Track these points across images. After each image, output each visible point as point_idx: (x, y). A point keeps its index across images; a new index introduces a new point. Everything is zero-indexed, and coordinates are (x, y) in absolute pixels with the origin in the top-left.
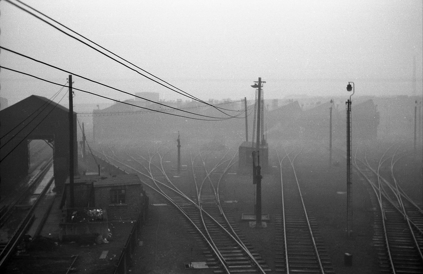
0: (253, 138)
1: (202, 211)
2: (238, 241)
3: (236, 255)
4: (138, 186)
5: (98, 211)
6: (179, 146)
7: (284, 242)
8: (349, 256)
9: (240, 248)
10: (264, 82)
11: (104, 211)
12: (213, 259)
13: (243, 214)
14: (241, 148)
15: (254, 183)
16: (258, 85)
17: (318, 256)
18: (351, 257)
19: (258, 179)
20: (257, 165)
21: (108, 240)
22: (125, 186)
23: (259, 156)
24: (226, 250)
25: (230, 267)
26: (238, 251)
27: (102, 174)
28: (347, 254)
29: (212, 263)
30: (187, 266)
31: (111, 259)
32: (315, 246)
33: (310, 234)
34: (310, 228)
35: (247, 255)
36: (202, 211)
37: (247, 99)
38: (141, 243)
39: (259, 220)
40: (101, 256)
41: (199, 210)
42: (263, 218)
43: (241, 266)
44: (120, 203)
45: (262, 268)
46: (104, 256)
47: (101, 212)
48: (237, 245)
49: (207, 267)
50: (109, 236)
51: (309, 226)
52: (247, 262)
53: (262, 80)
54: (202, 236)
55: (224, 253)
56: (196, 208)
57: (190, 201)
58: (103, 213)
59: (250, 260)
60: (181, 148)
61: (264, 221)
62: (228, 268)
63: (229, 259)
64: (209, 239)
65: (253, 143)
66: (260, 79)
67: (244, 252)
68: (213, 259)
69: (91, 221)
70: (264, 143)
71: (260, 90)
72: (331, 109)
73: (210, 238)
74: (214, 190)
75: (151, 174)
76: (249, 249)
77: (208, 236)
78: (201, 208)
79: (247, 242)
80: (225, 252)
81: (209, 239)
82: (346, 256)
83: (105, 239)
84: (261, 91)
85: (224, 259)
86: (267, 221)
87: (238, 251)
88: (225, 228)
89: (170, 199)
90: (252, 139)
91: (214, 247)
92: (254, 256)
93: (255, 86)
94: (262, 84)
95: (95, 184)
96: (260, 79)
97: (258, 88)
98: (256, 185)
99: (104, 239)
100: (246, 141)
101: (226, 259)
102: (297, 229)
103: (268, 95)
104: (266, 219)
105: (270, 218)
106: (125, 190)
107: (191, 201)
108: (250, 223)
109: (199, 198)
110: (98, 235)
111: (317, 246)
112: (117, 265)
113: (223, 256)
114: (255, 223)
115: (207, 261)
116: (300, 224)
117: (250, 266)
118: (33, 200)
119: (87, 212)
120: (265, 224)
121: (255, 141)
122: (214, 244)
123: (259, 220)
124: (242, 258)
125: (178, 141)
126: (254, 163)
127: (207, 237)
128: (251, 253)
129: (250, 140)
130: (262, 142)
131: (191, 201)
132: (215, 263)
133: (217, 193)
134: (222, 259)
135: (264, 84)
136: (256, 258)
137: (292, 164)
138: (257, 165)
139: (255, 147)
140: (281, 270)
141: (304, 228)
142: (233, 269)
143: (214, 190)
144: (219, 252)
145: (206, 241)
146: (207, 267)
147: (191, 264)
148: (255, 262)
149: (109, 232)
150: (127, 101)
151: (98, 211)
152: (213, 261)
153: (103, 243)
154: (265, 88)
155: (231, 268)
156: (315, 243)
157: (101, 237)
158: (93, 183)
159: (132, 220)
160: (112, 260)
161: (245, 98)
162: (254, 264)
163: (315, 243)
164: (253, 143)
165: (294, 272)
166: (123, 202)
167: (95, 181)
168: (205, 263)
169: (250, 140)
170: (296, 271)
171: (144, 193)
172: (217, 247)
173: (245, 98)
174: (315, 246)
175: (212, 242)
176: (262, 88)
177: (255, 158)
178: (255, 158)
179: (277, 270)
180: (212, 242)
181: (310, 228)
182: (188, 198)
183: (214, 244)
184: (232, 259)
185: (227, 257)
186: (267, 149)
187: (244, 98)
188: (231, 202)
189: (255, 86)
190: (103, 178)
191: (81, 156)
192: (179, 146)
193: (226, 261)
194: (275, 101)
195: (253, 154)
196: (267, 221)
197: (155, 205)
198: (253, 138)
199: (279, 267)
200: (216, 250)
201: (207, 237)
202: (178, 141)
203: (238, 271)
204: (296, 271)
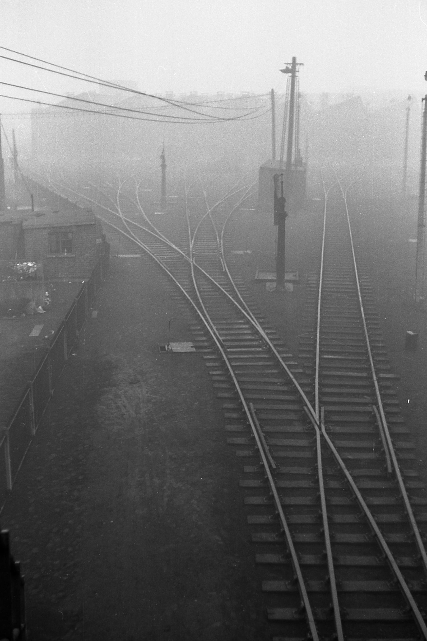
0: (282, 154)
1: (194, 265)
2: (246, 311)
3: (239, 332)
4: (93, 227)
5: (30, 264)
6: (164, 166)
7: (317, 313)
8: (413, 335)
9: (248, 322)
10: (301, 64)
11: (40, 265)
12: (204, 338)
13: (257, 271)
14: (262, 169)
15: (275, 224)
16: (291, 70)
17: (367, 335)
18: (416, 336)
19: (281, 217)
20: (280, 196)
21: (44, 309)
22: (71, 226)
23: (282, 182)
24: (226, 324)
25: (229, 350)
26: (244, 326)
27: (36, 209)
28: (411, 333)
29: (202, 344)
30: (163, 348)
31: (46, 337)
32: (364, 321)
33: (359, 301)
34: (359, 293)
35: (257, 332)
36: (194, 265)
37: (275, 91)
38: (95, 314)
39: (280, 280)
40: (32, 333)
41: (190, 264)
42: (288, 276)
43: (246, 349)
44: (64, 252)
45: (278, 352)
46: (36, 332)
47: (34, 267)
48: (244, 317)
49: (194, 350)
50: (46, 303)
51: (359, 289)
52: (254, 343)
53: (298, 61)
54: (191, 303)
55: (223, 329)
56: (186, 261)
57: (177, 251)
58: (37, 267)
59: (261, 340)
60: (167, 169)
61: (289, 281)
62: (225, 352)
63: (228, 338)
64: (201, 309)
65: (281, 160)
66: (294, 59)
67: (252, 327)
68: (204, 338)
69: (19, 280)
70: (299, 161)
71: (294, 77)
72: (408, 109)
73: (245, 305)
74: (217, 233)
75: (119, 209)
76: (261, 324)
77: (199, 303)
78: (192, 261)
79: (260, 314)
80: (224, 327)
81: (201, 309)
82: (408, 334)
83: (40, 307)
84: (297, 79)
85: (221, 339)
86: (294, 282)
87: (244, 326)
88: (227, 291)
89: (146, 248)
90: (281, 156)
91: (207, 320)
92: (267, 334)
93: (285, 71)
94: (297, 67)
95: (25, 223)
96: (294, 59)
97: (290, 74)
98: (277, 227)
99: (38, 307)
100: (271, 159)
101: (224, 338)
102: (339, 295)
103: (309, 84)
104: (294, 278)
105: (299, 276)
106: (72, 233)
107: (179, 250)
108: (268, 284)
109: (191, 246)
110: (28, 301)
111: (366, 319)
112: (50, 346)
113: (219, 334)
114: (275, 284)
115: (194, 341)
116: (346, 286)
117: (260, 349)
118: (66, 250)
119: (13, 266)
120: (290, 287)
121: (285, 159)
122: (208, 316)
123: (280, 280)
124: (249, 337)
125: (163, 157)
126: (275, 192)
127: (198, 304)
128: (264, 329)
129: (278, 158)
130: (296, 160)
131: (179, 250)
132: (206, 344)
133: (220, 239)
134: (218, 339)
135: (301, 67)
136: (271, 337)
137: (344, 196)
138: (280, 196)
139: (284, 168)
140: (308, 356)
141: (349, 292)
142: (233, 353)
143: (217, 233)
144: (214, 328)
145: (196, 311)
146: (194, 350)
147: (168, 345)
148: (268, 344)
149: (48, 297)
150: (85, 94)
151: (30, 264)
152: (203, 341)
153: (36, 314)
154: (302, 73)
155: (230, 352)
156: (363, 316)
157: (33, 304)
158: (22, 222)
159: (84, 278)
160: (48, 339)
161: (273, 90)
162: (266, 346)
163: (363, 316)
164: (281, 160)
165: (326, 359)
166: (69, 251)
167: (26, 220)
168: (190, 344)
169: (278, 158)
170: (330, 357)
171: (103, 238)
172: (212, 321)
173: (273, 90)
174: (364, 321)
175: (206, 312)
176: (297, 74)
177: (281, 186)
178: (281, 186)
179: (300, 356)
180: (206, 312)
181: (359, 293)
182: (174, 246)
183: (208, 316)
184: (233, 338)
185: (226, 335)
186: (305, 172)
187: (270, 90)
188: (242, 252)
189: (285, 71)
190: (38, 215)
191: (13, 181)
192: (164, 166)
193: (223, 341)
194: (325, 96)
195: (276, 178)
196: (294, 282)
197: (121, 256)
198: (282, 154)
199: (304, 351)
200: (209, 324)
201: (198, 304)
202: (163, 157)
203: (242, 356)
204: (330, 357)
